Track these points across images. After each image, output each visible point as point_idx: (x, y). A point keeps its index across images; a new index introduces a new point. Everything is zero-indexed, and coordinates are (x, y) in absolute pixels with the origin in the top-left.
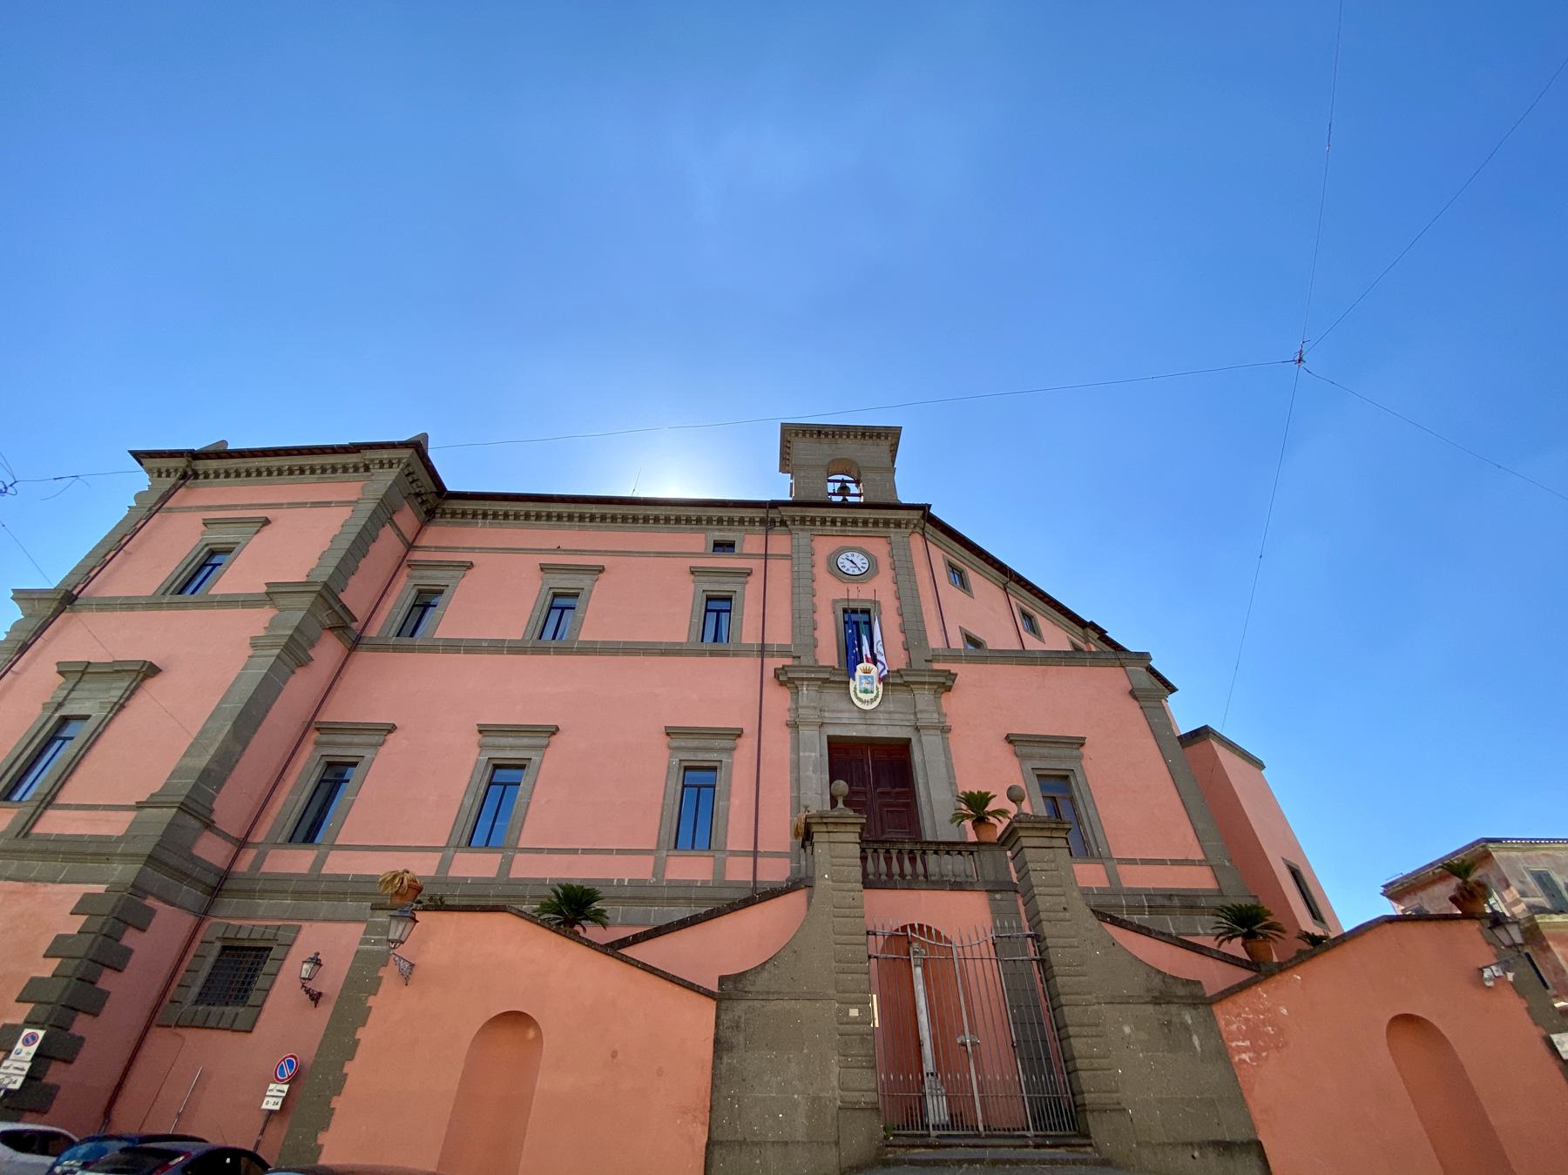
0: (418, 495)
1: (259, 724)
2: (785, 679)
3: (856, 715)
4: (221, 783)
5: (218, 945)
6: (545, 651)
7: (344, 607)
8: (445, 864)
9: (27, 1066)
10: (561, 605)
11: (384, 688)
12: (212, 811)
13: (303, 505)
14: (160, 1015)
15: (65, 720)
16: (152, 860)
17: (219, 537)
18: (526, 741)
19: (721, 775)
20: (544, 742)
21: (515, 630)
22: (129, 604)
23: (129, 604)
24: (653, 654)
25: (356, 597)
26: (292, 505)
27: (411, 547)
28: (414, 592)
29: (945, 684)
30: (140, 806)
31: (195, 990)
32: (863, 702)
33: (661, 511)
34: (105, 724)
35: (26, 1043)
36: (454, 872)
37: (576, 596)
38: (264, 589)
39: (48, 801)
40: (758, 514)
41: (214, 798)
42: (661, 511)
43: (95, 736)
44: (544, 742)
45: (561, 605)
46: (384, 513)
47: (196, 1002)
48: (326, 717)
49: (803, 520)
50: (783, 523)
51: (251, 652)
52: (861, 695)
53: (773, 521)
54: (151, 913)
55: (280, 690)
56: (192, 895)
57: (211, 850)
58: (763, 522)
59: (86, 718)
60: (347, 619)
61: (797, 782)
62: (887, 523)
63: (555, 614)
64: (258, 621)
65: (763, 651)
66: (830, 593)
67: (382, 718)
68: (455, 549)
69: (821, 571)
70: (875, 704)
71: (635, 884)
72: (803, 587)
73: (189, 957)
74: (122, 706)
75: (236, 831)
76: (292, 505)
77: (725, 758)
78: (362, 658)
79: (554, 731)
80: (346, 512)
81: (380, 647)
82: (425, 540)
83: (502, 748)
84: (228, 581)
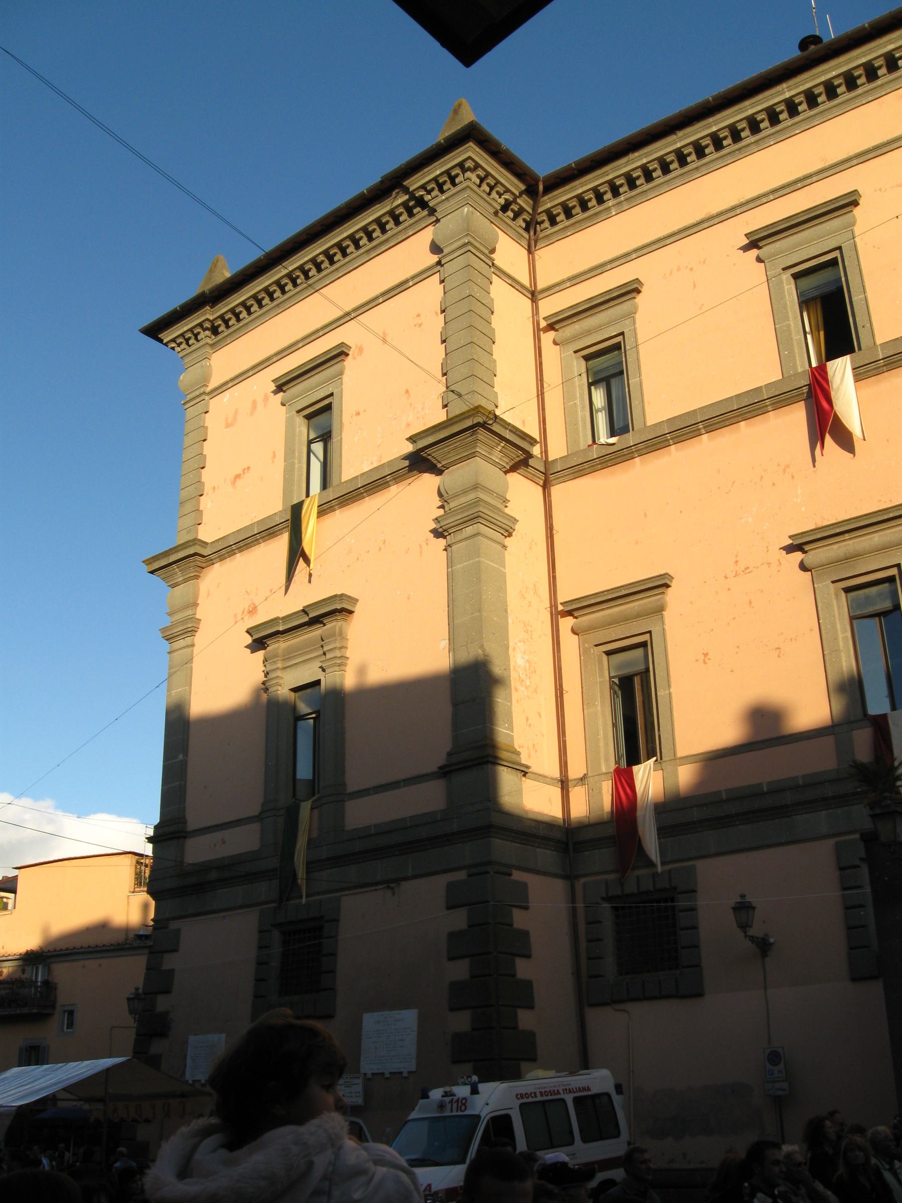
17: (310, 392)
79: (661, 584)
81: (579, 468)
84: (358, 455)
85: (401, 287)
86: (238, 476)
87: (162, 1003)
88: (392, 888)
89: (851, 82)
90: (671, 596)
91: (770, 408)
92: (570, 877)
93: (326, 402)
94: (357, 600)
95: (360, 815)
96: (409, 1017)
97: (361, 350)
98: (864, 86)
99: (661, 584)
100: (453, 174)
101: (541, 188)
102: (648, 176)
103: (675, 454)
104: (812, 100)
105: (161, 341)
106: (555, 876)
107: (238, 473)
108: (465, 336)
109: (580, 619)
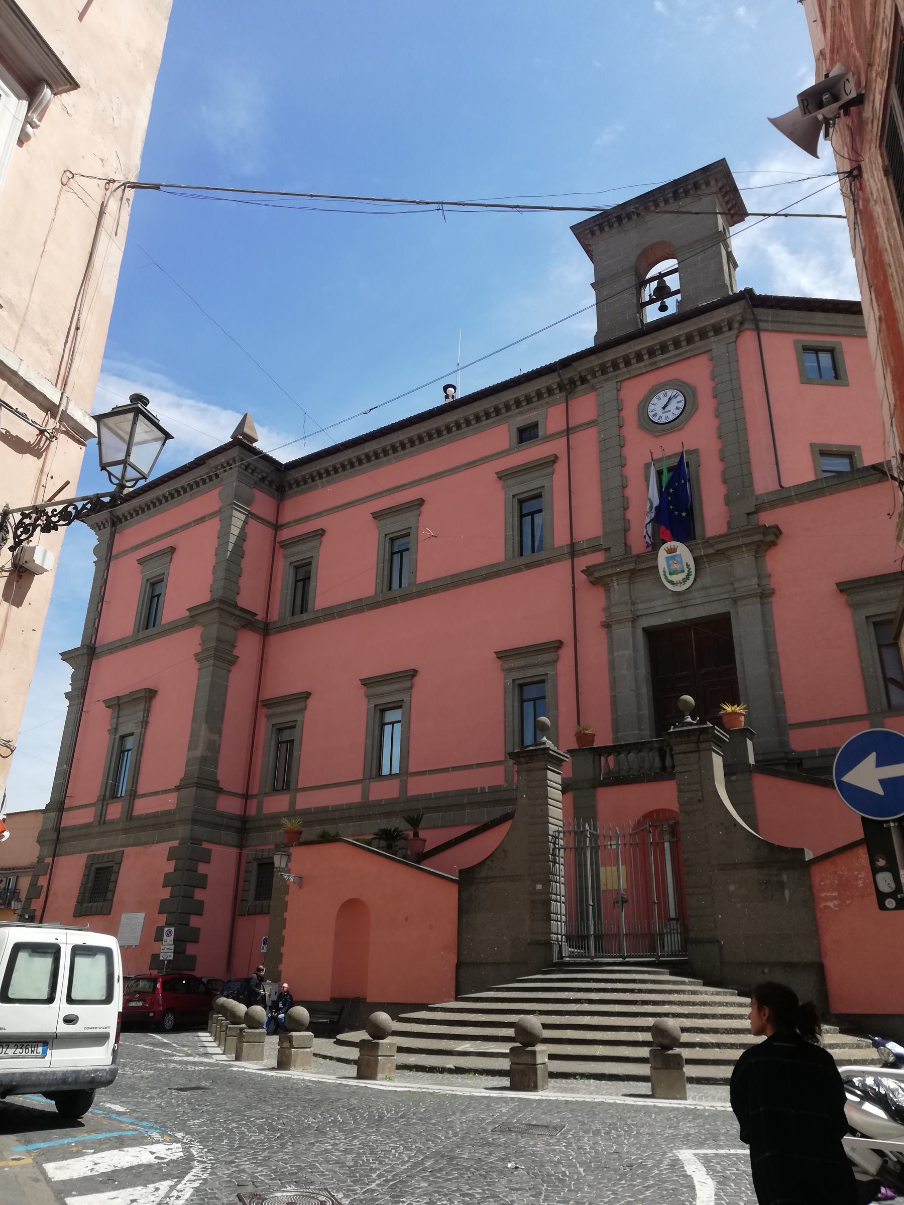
0: (263, 479)
1: (223, 717)
2: (597, 578)
3: (670, 599)
4: (215, 762)
5: (255, 864)
6: (392, 601)
7: (243, 610)
8: (366, 792)
9: (172, 947)
10: (397, 548)
12: (218, 782)
14: (238, 911)
15: (123, 737)
16: (194, 821)
17: (153, 570)
18: (396, 686)
19: (548, 686)
20: (408, 684)
21: (366, 585)
24: (477, 581)
25: (250, 598)
27: (277, 527)
28: (292, 570)
29: (771, 537)
30: (178, 789)
31: (252, 892)
32: (672, 583)
34: (143, 735)
35: (168, 935)
36: (372, 797)
37: (408, 535)
39: (133, 794)
40: (552, 380)
41: (216, 774)
43: (141, 747)
44: (408, 684)
45: (397, 548)
47: (256, 899)
48: (269, 693)
49: (604, 370)
50: (583, 380)
52: (670, 578)
53: (572, 382)
54: (210, 851)
55: (227, 687)
56: (231, 836)
57: (229, 806)
58: (561, 387)
59: (132, 734)
60: (249, 617)
61: (613, 682)
62: (703, 334)
63: (397, 558)
65: (573, 551)
66: (642, 453)
67: (298, 687)
68: (307, 518)
69: (632, 431)
70: (692, 578)
71: (494, 790)
72: (613, 456)
73: (242, 873)
74: (147, 723)
75: (239, 789)
77: (549, 670)
78: (276, 641)
79: (413, 673)
82: (288, 515)
83: (382, 695)
89: (439, 433)
90: (311, 702)
92: (241, 846)
95: (142, 807)
96: (141, 916)
98: (446, 436)
102: (328, 473)
104: (478, 419)
106: (234, 846)
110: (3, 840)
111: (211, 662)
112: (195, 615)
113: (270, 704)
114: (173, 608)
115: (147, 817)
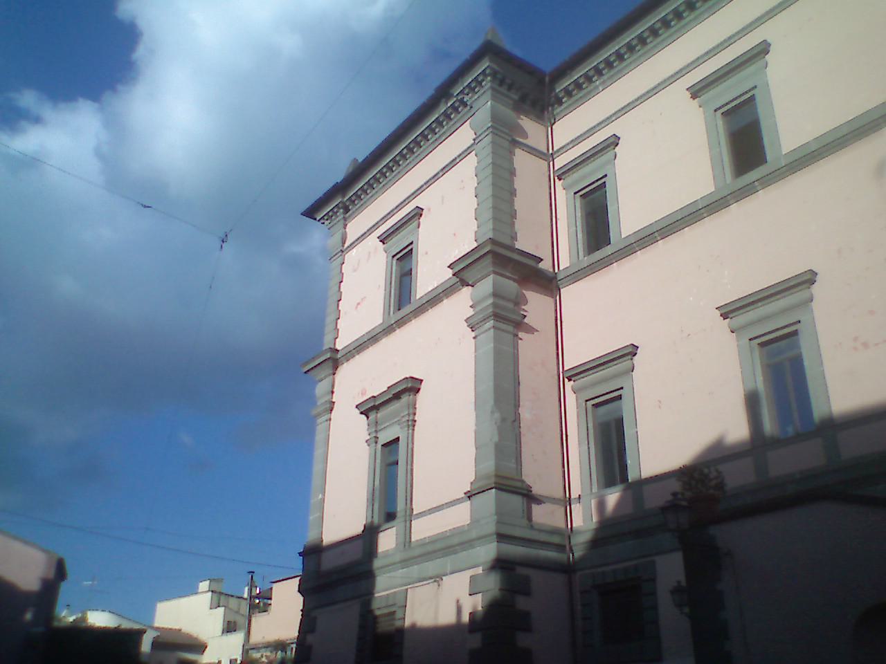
11: (591, 316)
13: (435, 177)
17: (398, 243)
19: (625, 404)
22: (373, 338)
23: (373, 338)
25: (529, 240)
26: (428, 183)
30: (470, 496)
33: (721, 48)
38: (450, 273)
39: (410, 516)
42: (721, 48)
46: (505, 139)
48: (571, 362)
51: (473, 334)
64: (462, 303)
76: (428, 183)
78: (569, 294)
80: (471, 161)
81: (577, 275)
84: (425, 283)
85: (453, 163)
86: (359, 304)
87: (522, 603)
88: (438, 582)
90: (423, 399)
91: (705, 215)
93: (409, 248)
94: (422, 381)
95: (422, 530)
97: (429, 210)
99: (632, 351)
100: (480, 80)
101: (547, 79)
103: (641, 257)
105: (315, 219)
107: (358, 301)
108: (501, 194)
109: (576, 382)
110: (62, 140)
111: (491, 323)
112: (463, 272)
113: (575, 374)
114: (431, 272)
115: (434, 540)
